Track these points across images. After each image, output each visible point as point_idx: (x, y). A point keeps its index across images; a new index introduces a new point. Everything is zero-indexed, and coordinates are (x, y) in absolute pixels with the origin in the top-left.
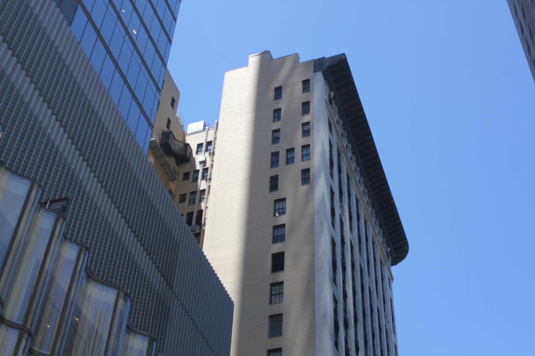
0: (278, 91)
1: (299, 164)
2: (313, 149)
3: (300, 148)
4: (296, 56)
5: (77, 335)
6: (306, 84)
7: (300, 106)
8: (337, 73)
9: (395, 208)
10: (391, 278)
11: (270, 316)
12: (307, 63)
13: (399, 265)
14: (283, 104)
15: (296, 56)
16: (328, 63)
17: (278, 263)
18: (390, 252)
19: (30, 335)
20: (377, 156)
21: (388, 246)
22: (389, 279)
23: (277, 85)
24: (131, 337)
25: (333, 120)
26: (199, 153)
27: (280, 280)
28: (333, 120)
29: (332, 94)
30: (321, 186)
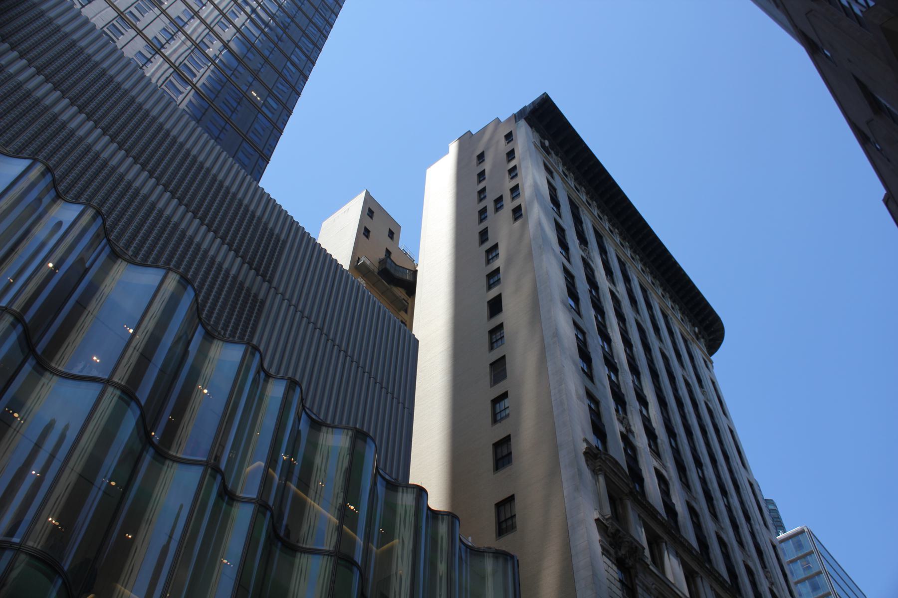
0: (481, 157)
1: (509, 205)
2: (523, 189)
3: (509, 192)
4: (498, 121)
5: (140, 350)
6: (509, 137)
7: (505, 156)
8: (544, 117)
9: (685, 274)
10: (712, 362)
11: (491, 365)
12: (509, 120)
13: (521, 107)
14: (487, 166)
15: (498, 121)
16: (528, 110)
17: (495, 306)
18: (700, 332)
19: (279, 538)
20: (661, 244)
21: (694, 325)
22: (705, 362)
23: (479, 152)
24: (322, 434)
25: (549, 162)
26: (495, 345)
27: (499, 323)
28: (549, 162)
29: (547, 143)
30: (538, 215)
